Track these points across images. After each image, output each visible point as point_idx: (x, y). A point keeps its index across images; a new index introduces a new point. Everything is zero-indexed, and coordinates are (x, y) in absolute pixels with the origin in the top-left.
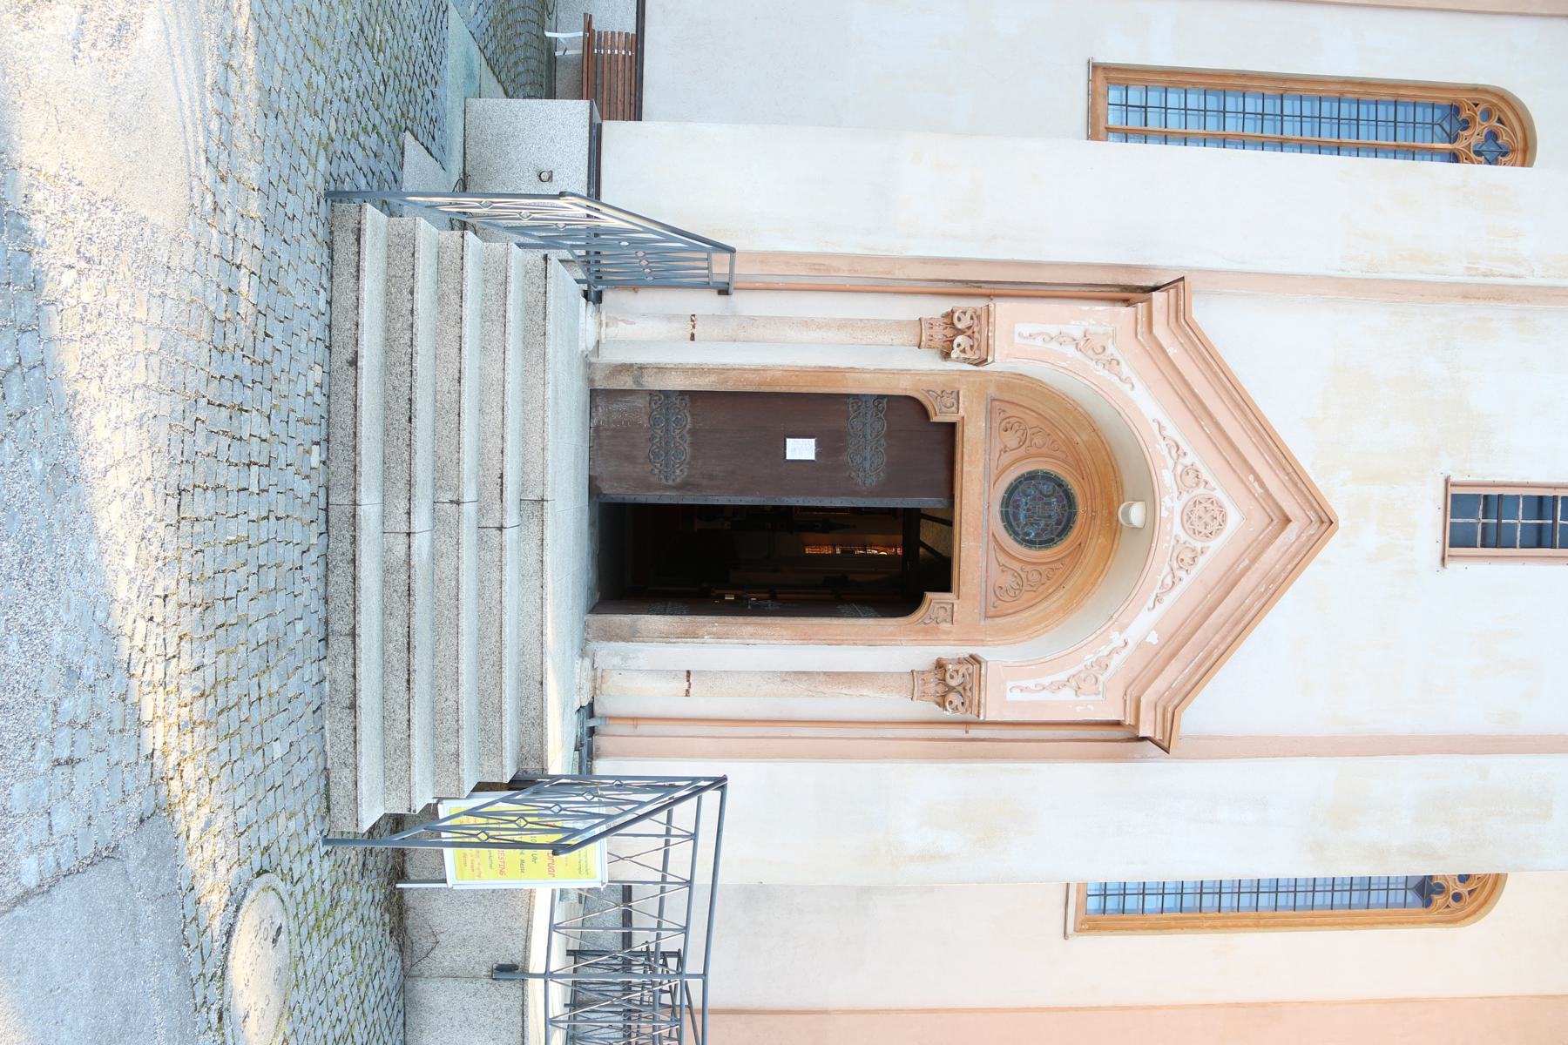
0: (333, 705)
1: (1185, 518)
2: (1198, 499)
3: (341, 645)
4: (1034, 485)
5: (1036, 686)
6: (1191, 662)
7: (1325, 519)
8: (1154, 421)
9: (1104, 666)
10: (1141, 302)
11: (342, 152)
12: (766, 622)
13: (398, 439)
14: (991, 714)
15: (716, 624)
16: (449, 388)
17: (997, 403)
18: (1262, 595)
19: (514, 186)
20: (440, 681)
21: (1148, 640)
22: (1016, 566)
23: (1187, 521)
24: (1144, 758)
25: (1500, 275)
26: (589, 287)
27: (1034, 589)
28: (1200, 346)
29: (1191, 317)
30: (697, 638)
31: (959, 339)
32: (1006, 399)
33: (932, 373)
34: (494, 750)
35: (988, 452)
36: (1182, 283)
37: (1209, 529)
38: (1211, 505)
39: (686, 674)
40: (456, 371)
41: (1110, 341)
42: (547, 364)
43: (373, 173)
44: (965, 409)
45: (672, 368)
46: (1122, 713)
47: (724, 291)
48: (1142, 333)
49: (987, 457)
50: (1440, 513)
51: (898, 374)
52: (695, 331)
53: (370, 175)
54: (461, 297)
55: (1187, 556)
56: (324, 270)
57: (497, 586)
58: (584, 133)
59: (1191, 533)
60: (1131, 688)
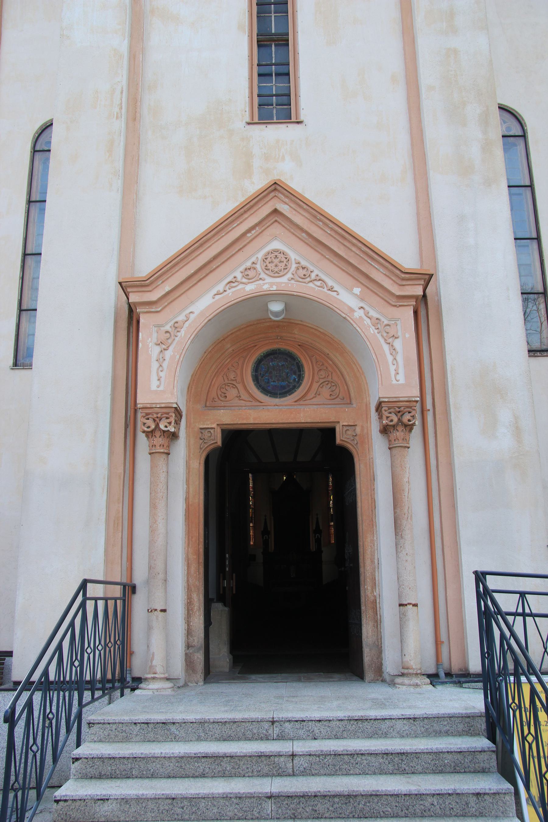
1: (276, 275)
2: (263, 267)
4: (262, 377)
5: (394, 365)
6: (371, 264)
7: (273, 187)
8: (213, 298)
9: (378, 321)
10: (137, 309)
12: (362, 552)
14: (415, 393)
16: (179, 808)
17: (208, 403)
18: (324, 223)
20: (418, 810)
21: (359, 294)
22: (315, 386)
23: (279, 273)
24: (438, 294)
25: (121, 100)
26: (128, 687)
27: (330, 373)
28: (163, 270)
29: (145, 277)
30: (376, 600)
31: (162, 427)
33: (188, 446)
34: (470, 758)
36: (122, 283)
37: (283, 259)
38: (268, 259)
39: (401, 607)
41: (162, 329)
44: (212, 423)
46: (409, 307)
49: (244, 408)
50: (270, 126)
52: (159, 609)
55: (301, 272)
57: (338, 758)
59: (286, 271)
60: (391, 302)
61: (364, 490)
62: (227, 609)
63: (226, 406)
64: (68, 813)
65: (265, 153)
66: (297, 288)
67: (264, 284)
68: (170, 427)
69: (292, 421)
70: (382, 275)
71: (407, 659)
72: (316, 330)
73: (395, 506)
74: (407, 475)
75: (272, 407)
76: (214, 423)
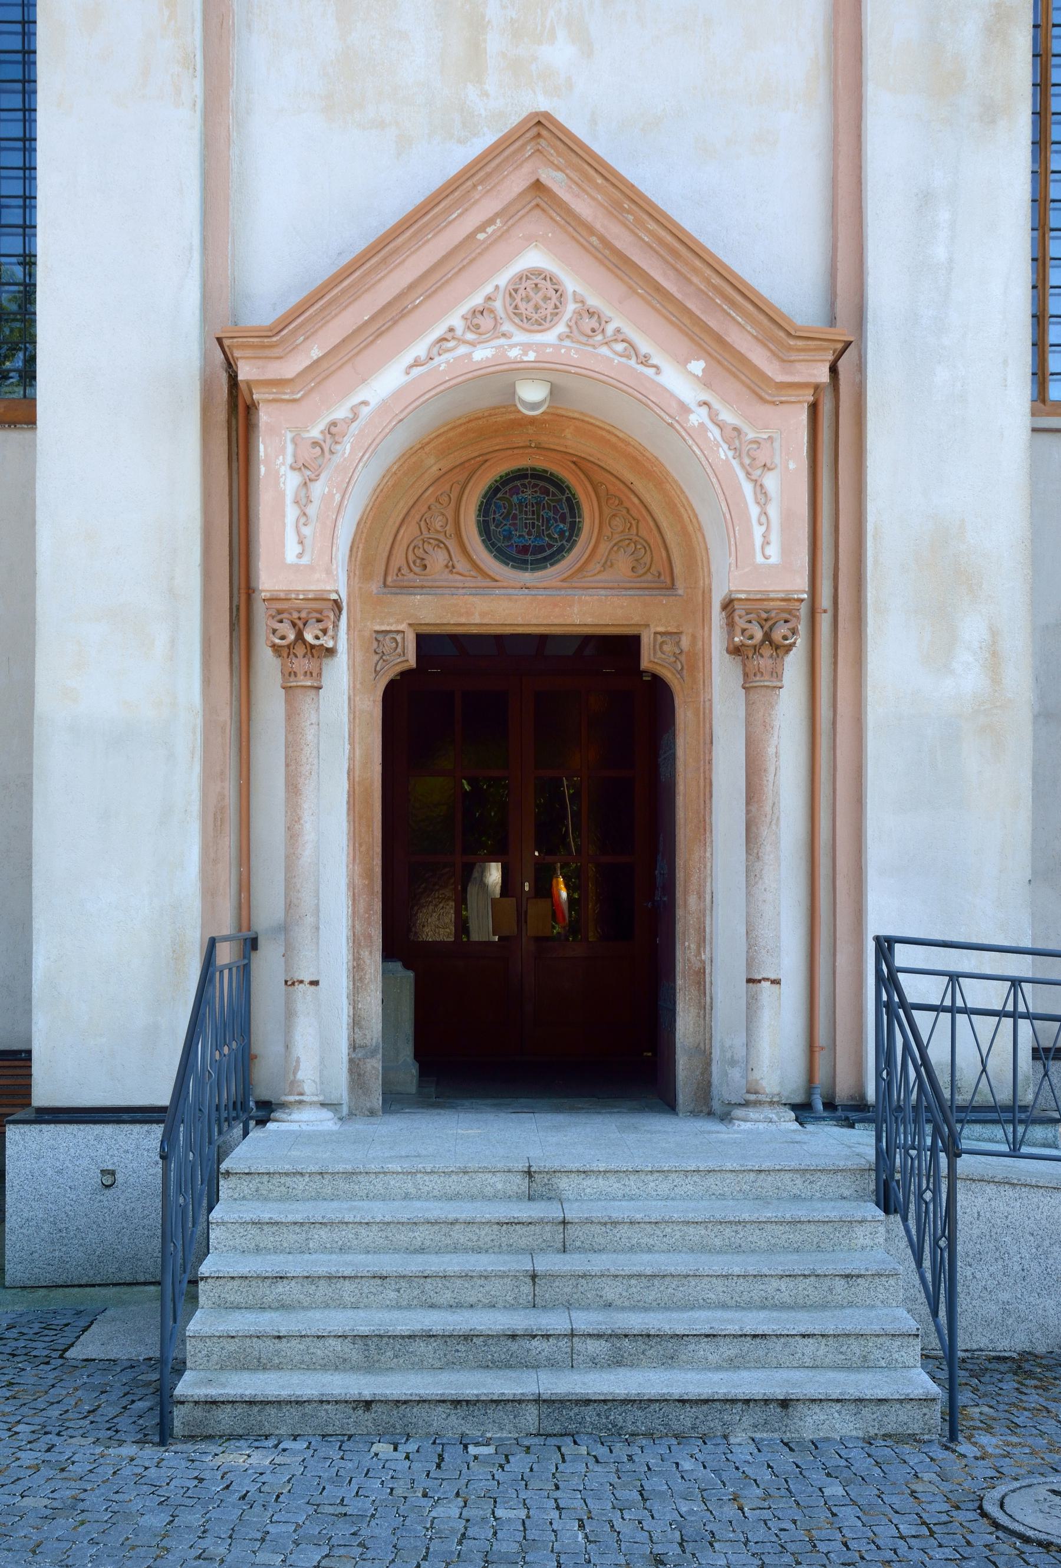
0: (784, 1429)
1: (536, 327)
2: (511, 288)
3: (710, 1418)
5: (761, 524)
6: (729, 314)
7: (535, 131)
11: (109, 1429)
13: (458, 1351)
14: (799, 584)
15: (687, 944)
16: (393, 1291)
17: (389, 579)
19: (120, 1220)
21: (700, 374)
22: (604, 548)
23: (540, 325)
26: (251, 1118)
30: (704, 968)
31: (309, 637)
32: (383, 568)
33: (352, 667)
35: (454, 591)
39: (751, 984)
40: (372, 1282)
42: (357, 1170)
43: (128, 1393)
44: (398, 622)
45: (354, 1008)
46: (799, 405)
47: (252, 944)
48: (293, 393)
49: (461, 591)
51: (354, 712)
52: (307, 980)
53: (130, 1397)
54: (281, 1278)
55: (588, 323)
56: (257, 1444)
58: (49, 1131)
61: (691, 760)
62: (411, 974)
63: (425, 587)
64: (222, 1296)
65: (512, 18)
66: (573, 354)
67: (511, 346)
68: (325, 638)
69: (557, 621)
70: (750, 338)
71: (756, 1075)
72: (609, 432)
73: (749, 800)
74: (774, 741)
75: (516, 592)
76: (402, 623)
